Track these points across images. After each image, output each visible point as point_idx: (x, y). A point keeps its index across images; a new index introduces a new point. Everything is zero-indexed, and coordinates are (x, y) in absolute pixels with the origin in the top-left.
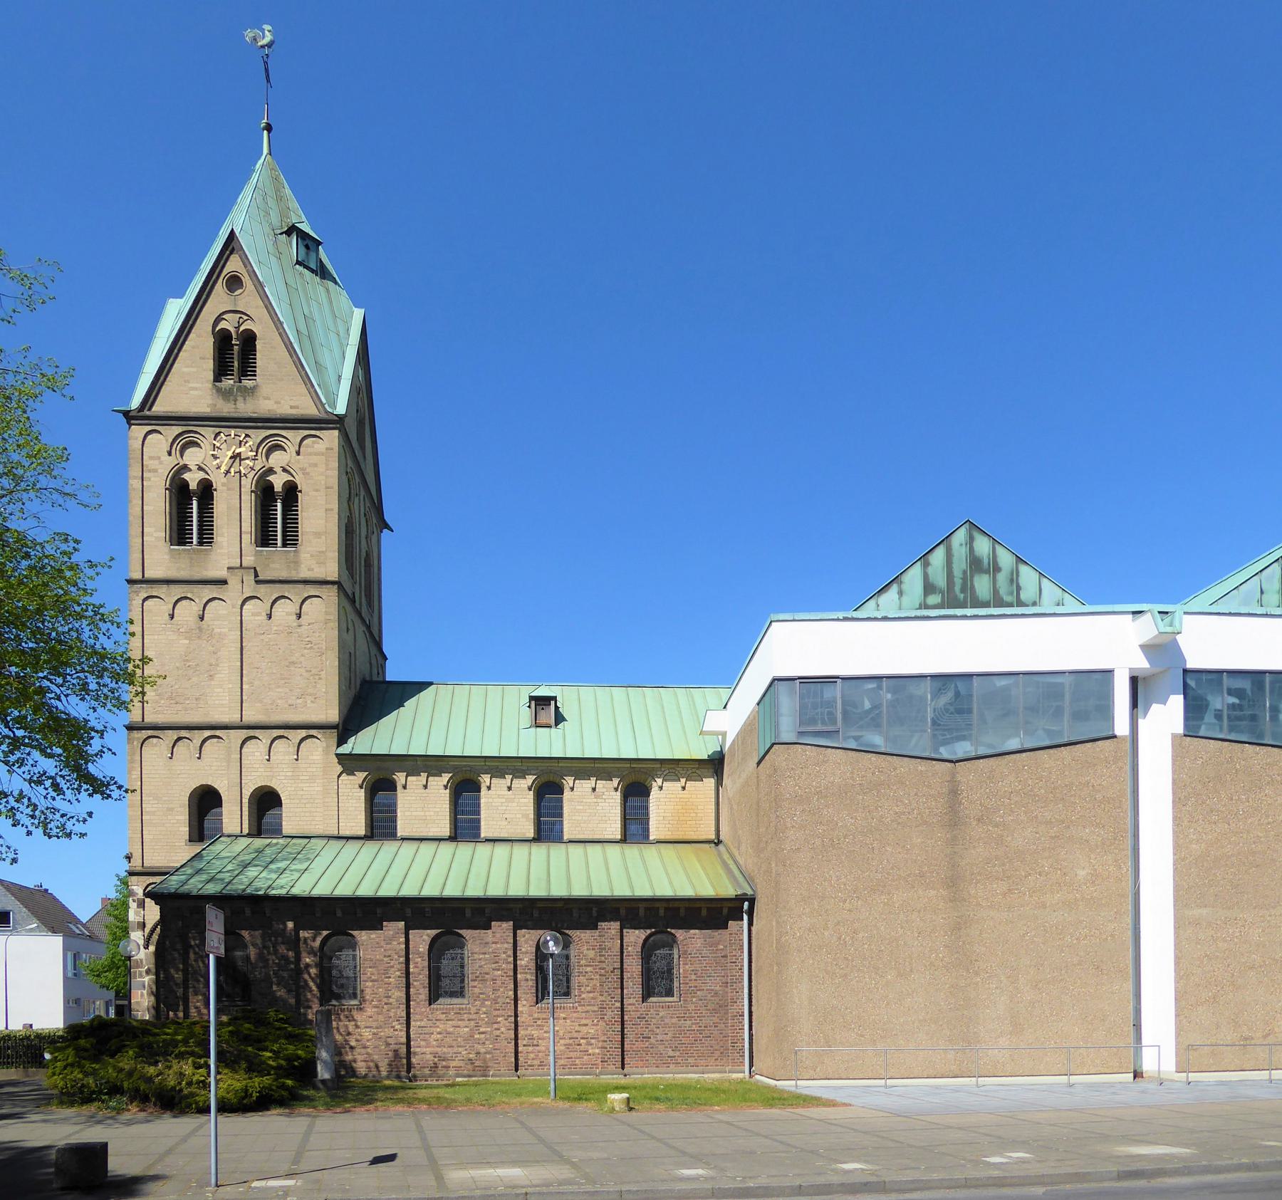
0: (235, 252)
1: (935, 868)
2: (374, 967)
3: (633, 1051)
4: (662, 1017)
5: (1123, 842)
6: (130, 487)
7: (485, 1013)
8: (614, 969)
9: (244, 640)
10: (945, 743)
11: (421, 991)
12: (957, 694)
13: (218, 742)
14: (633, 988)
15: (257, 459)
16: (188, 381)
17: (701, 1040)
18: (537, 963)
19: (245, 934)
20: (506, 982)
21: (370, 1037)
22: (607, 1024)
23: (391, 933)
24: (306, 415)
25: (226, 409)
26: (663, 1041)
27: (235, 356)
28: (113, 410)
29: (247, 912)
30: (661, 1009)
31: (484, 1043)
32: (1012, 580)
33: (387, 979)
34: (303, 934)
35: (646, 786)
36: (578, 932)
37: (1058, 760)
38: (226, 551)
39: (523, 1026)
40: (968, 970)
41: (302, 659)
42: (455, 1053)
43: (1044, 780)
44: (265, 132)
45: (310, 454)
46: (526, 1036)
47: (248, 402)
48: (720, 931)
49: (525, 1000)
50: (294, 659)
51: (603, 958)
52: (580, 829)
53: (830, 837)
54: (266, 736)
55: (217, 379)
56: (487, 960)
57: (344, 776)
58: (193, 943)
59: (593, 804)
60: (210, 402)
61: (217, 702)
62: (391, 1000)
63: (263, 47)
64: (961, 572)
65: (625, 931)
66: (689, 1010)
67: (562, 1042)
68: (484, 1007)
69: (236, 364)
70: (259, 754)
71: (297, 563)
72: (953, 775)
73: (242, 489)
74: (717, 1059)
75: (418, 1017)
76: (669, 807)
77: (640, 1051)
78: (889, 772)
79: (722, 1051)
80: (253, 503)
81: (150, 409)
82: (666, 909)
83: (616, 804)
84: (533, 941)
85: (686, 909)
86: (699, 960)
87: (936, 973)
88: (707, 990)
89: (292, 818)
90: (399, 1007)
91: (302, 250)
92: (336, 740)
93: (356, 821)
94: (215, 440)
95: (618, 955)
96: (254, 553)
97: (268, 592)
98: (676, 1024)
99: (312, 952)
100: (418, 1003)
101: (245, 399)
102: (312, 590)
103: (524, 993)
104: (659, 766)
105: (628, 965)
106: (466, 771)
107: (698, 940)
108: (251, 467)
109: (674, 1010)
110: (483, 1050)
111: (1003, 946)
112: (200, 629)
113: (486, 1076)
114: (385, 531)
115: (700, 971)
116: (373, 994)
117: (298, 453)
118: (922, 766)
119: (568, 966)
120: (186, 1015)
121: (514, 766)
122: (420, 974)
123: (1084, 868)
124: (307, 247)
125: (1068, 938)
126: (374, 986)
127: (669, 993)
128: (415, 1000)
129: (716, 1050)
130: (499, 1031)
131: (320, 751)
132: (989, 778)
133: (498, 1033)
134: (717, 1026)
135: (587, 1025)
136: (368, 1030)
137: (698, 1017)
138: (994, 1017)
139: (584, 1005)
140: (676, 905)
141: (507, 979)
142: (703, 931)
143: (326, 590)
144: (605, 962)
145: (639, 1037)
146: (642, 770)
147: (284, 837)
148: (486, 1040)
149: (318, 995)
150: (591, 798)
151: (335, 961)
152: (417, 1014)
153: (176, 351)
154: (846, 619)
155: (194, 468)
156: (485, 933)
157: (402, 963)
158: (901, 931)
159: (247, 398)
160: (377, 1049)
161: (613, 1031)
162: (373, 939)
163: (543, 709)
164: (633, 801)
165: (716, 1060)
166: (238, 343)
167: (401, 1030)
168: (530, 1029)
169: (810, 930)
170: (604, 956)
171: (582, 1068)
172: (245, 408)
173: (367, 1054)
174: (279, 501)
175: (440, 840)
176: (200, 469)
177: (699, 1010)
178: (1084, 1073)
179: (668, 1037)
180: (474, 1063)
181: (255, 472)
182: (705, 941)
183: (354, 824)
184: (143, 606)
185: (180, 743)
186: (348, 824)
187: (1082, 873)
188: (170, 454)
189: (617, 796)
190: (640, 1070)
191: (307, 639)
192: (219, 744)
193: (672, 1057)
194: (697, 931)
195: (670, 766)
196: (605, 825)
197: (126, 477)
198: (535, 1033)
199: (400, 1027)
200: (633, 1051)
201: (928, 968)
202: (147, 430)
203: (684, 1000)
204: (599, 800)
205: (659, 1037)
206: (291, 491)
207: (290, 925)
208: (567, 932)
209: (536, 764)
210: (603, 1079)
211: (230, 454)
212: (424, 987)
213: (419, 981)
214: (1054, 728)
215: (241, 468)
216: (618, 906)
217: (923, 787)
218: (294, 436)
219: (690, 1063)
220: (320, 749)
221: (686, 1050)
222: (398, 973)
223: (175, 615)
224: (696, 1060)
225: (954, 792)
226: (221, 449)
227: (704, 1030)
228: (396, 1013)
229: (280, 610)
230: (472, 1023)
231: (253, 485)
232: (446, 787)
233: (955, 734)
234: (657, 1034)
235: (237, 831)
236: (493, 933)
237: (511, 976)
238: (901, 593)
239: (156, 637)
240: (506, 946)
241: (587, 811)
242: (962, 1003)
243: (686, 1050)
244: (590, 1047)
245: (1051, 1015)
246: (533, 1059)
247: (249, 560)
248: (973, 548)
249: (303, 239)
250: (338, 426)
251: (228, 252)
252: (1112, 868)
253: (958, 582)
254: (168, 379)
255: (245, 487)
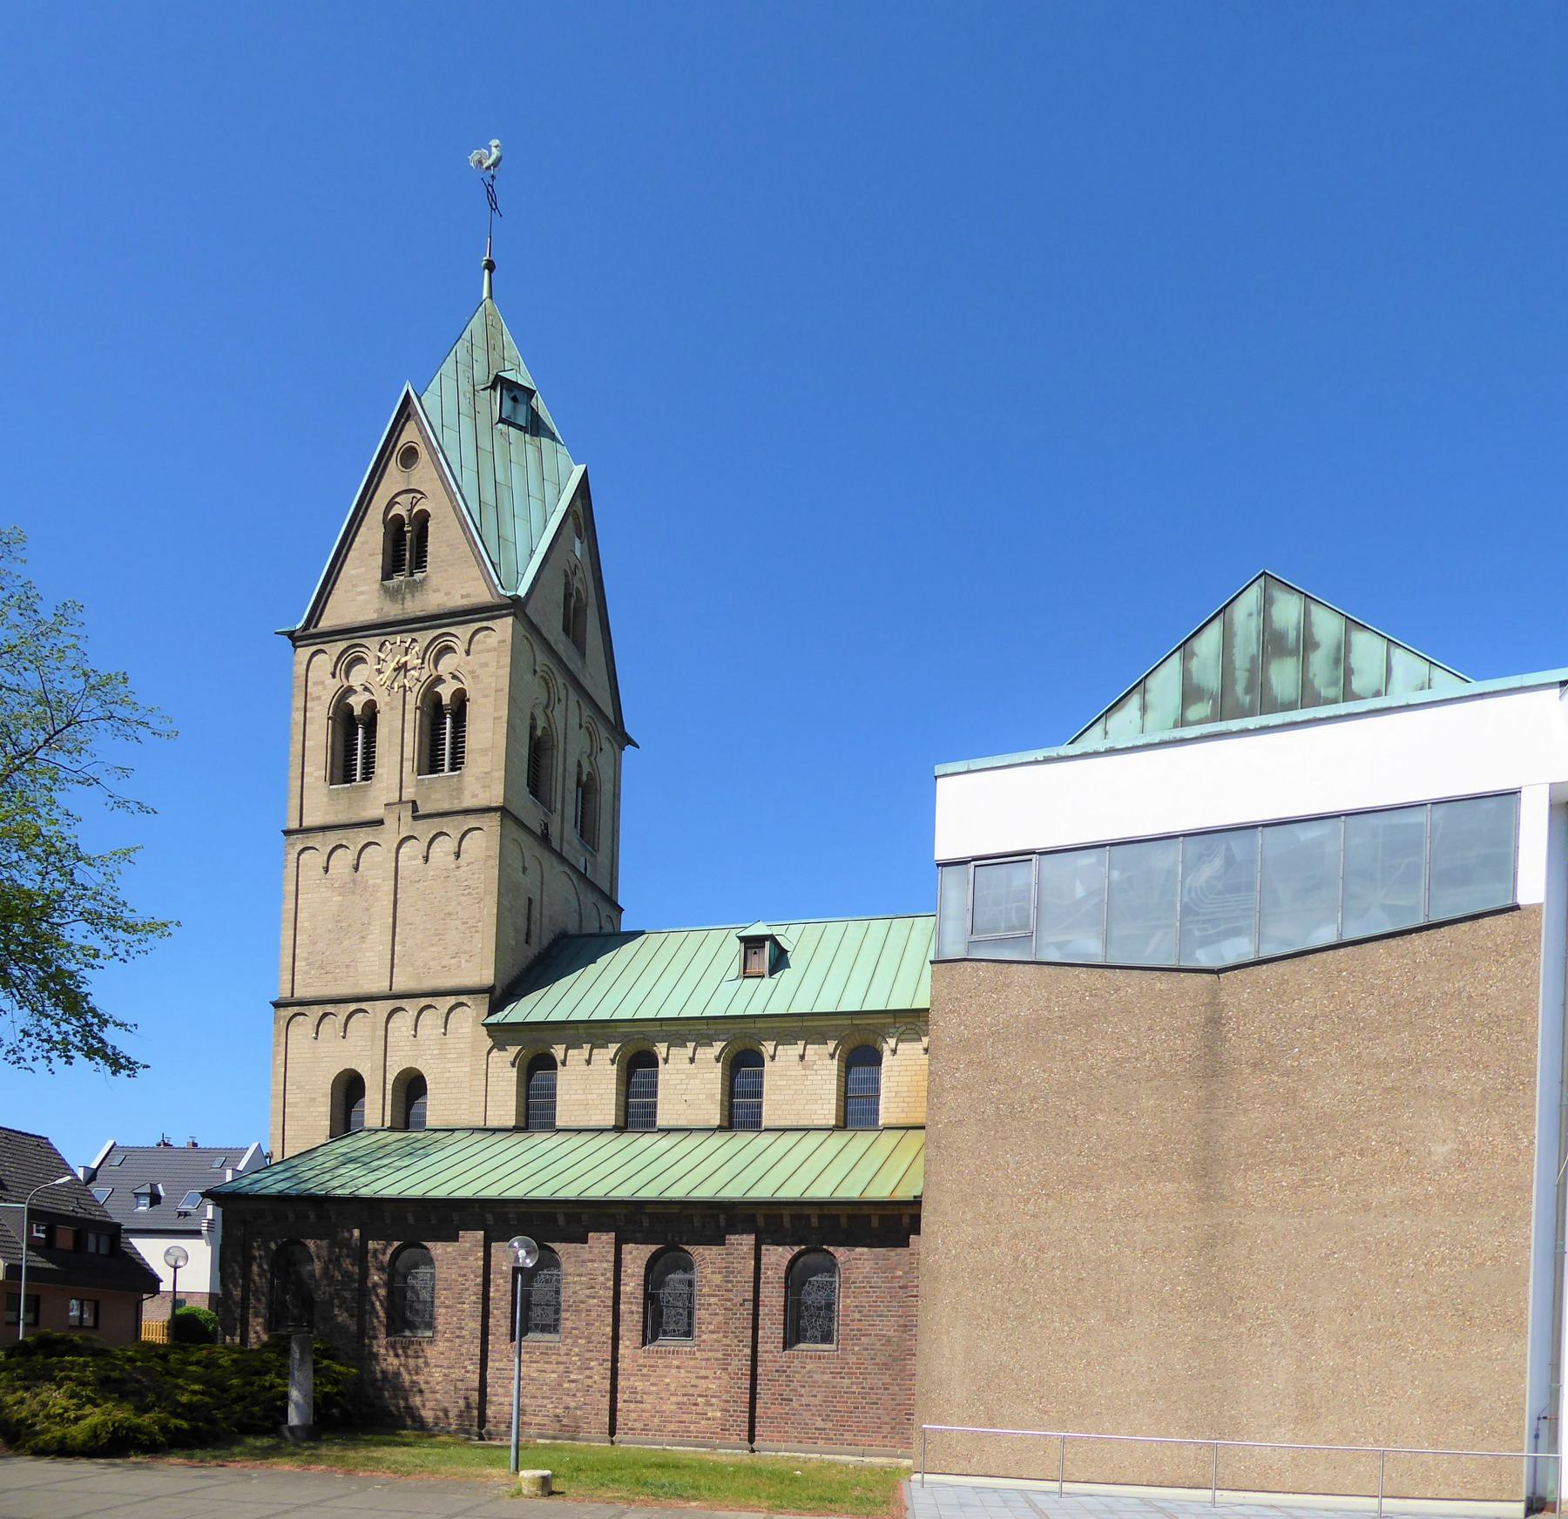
0: (411, 418)
1: (1177, 1146)
2: (449, 1289)
3: (768, 1418)
4: (809, 1372)
5: (1525, 1093)
6: (292, 721)
7: (577, 1355)
8: (744, 1300)
9: (399, 891)
10: (1205, 942)
11: (502, 1322)
12: (1230, 862)
13: (364, 1017)
14: (771, 1328)
15: (423, 668)
16: (355, 586)
17: (864, 1408)
18: (646, 1290)
19: (311, 1244)
20: (603, 1314)
21: (440, 1379)
22: (731, 1378)
23: (468, 1245)
24: (480, 603)
25: (394, 611)
26: (809, 1405)
27: (408, 547)
28: (276, 633)
29: (311, 1217)
30: (808, 1361)
31: (574, 1395)
32: (1337, 661)
33: (460, 1306)
34: (372, 1245)
35: (877, 1051)
36: (701, 1249)
37: (1403, 957)
38: (385, 785)
39: (624, 1374)
40: (1225, 1315)
41: (459, 908)
42: (539, 1406)
43: (1376, 993)
44: (486, 271)
45: (482, 651)
46: (627, 1388)
47: (416, 598)
48: (899, 1250)
49: (629, 1339)
50: (450, 909)
51: (730, 1285)
52: (780, 1112)
53: (1009, 1101)
54: (412, 1006)
55: (387, 575)
56: (582, 1284)
57: (495, 1053)
58: (257, 1254)
59: (799, 1078)
60: (377, 606)
61: (367, 969)
62: (464, 1332)
63: (488, 168)
64: (1248, 660)
65: (763, 1247)
66: (848, 1364)
67: (673, 1399)
68: (576, 1346)
69: (408, 556)
70: (405, 1029)
71: (460, 790)
72: (1215, 994)
73: (406, 707)
74: (886, 1437)
75: (497, 1356)
76: (906, 1079)
77: (777, 1418)
78: (1108, 995)
79: (894, 1425)
80: (417, 722)
81: (315, 626)
82: (820, 1217)
83: (831, 1077)
84: (641, 1259)
85: (881, 1217)
86: (866, 1292)
87: (1171, 1316)
88: (876, 1335)
89: (436, 1109)
90: (472, 1342)
91: (508, 403)
92: (487, 1007)
93: (506, 1108)
94: (380, 651)
95: (751, 1282)
96: (415, 783)
97: (425, 829)
98: (828, 1382)
99: (381, 1269)
100: (497, 1338)
101: (413, 596)
102: (472, 822)
103: (627, 1330)
104: (892, 1020)
105: (765, 1297)
106: (638, 1039)
107: (866, 1262)
108: (416, 679)
109: (827, 1363)
110: (573, 1404)
111: (1289, 1272)
112: (354, 881)
113: (574, 1439)
114: (629, 748)
115: (867, 1308)
116: (446, 1324)
117: (468, 653)
118: (1163, 983)
119: (690, 1297)
120: (244, 1339)
121: (699, 1030)
122: (501, 1300)
123: (1444, 1141)
124: (515, 399)
125: (1409, 1263)
126: (447, 1313)
127: (827, 1338)
128: (494, 1334)
129: (885, 1423)
130: (591, 1380)
131: (470, 1020)
132: (1276, 994)
133: (589, 1382)
134: (888, 1389)
135: (707, 1377)
136: (438, 1369)
137: (860, 1374)
138: (1267, 1391)
139: (704, 1350)
140: (865, 1211)
141: (605, 1310)
142: (874, 1249)
143: (488, 820)
144: (732, 1291)
145: (777, 1399)
146: (868, 1027)
147: (426, 1130)
148: (578, 1390)
149: (385, 1322)
150: (797, 1070)
151: (410, 1281)
152: (496, 1351)
153: (344, 551)
154: (1047, 760)
155: (359, 689)
156: (582, 1248)
157: (478, 1285)
158: (1114, 1248)
159: (416, 595)
160: (447, 1395)
161: (738, 1388)
162: (449, 1253)
163: (755, 953)
164: (859, 1072)
165: (883, 1437)
166: (410, 528)
167: (474, 1372)
168: (632, 1379)
169: (971, 1246)
170: (731, 1282)
171: (697, 1437)
172: (415, 606)
173: (436, 1400)
174: (448, 716)
175: (602, 1131)
176: (366, 689)
177: (863, 1364)
178: (1429, 1495)
179: (817, 1401)
180: (561, 1421)
181: (421, 684)
182: (877, 1264)
183: (503, 1113)
184: (298, 859)
185: (326, 1020)
186: (497, 1113)
187: (1440, 1151)
188: (334, 675)
189: (833, 1066)
190: (776, 1445)
191: (466, 883)
192: (366, 1020)
193: (821, 1429)
194: (866, 1249)
195: (906, 1020)
196: (815, 1107)
197: (289, 709)
198: (639, 1385)
199: (473, 1367)
200: (768, 1418)
201: (1157, 1308)
202: (312, 651)
203: (842, 1349)
204: (808, 1072)
205: (805, 1400)
206: (460, 698)
207: (356, 1232)
208: (686, 1247)
209: (727, 1026)
210: (721, 1454)
211: (393, 665)
212: (506, 1317)
213: (500, 1308)
214: (1402, 903)
215: (406, 681)
216: (753, 1212)
217: (1162, 1016)
218: (463, 632)
219: (847, 1440)
220: (471, 1019)
221: (842, 1421)
222: (473, 1298)
223: (330, 867)
224: (855, 1435)
225: (1215, 1022)
226: (386, 662)
227: (869, 1394)
228: (468, 1350)
229: (439, 850)
230: (562, 1367)
231: (419, 700)
232: (613, 1062)
233: (1223, 927)
234: (802, 1396)
235: (378, 1125)
236: (590, 1247)
237: (609, 1306)
238: (1144, 708)
239: (310, 896)
240: (605, 1265)
241: (792, 1087)
242: (1212, 1366)
243: (842, 1421)
244: (709, 1408)
245: (1371, 1393)
246: (635, 1420)
247: (409, 794)
248: (1271, 616)
249: (509, 390)
250: (512, 610)
251: (403, 420)
252: (1499, 1139)
253: (1241, 677)
254: (336, 586)
255: (409, 704)
